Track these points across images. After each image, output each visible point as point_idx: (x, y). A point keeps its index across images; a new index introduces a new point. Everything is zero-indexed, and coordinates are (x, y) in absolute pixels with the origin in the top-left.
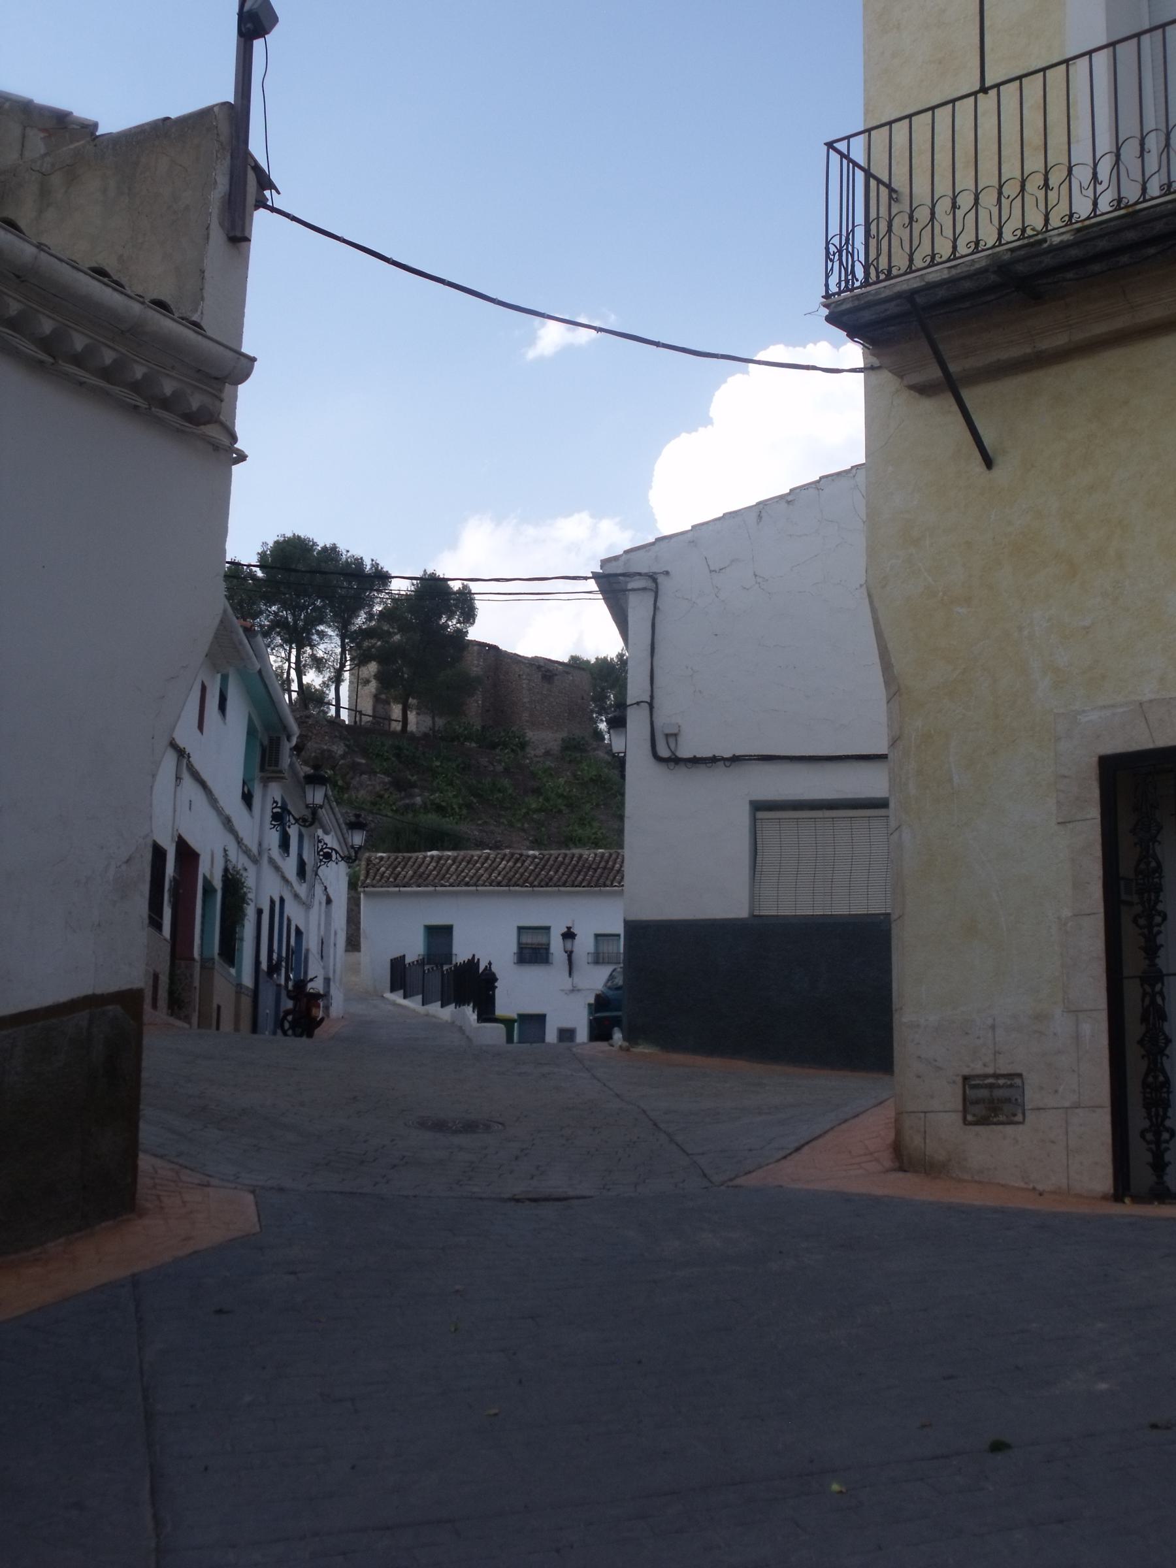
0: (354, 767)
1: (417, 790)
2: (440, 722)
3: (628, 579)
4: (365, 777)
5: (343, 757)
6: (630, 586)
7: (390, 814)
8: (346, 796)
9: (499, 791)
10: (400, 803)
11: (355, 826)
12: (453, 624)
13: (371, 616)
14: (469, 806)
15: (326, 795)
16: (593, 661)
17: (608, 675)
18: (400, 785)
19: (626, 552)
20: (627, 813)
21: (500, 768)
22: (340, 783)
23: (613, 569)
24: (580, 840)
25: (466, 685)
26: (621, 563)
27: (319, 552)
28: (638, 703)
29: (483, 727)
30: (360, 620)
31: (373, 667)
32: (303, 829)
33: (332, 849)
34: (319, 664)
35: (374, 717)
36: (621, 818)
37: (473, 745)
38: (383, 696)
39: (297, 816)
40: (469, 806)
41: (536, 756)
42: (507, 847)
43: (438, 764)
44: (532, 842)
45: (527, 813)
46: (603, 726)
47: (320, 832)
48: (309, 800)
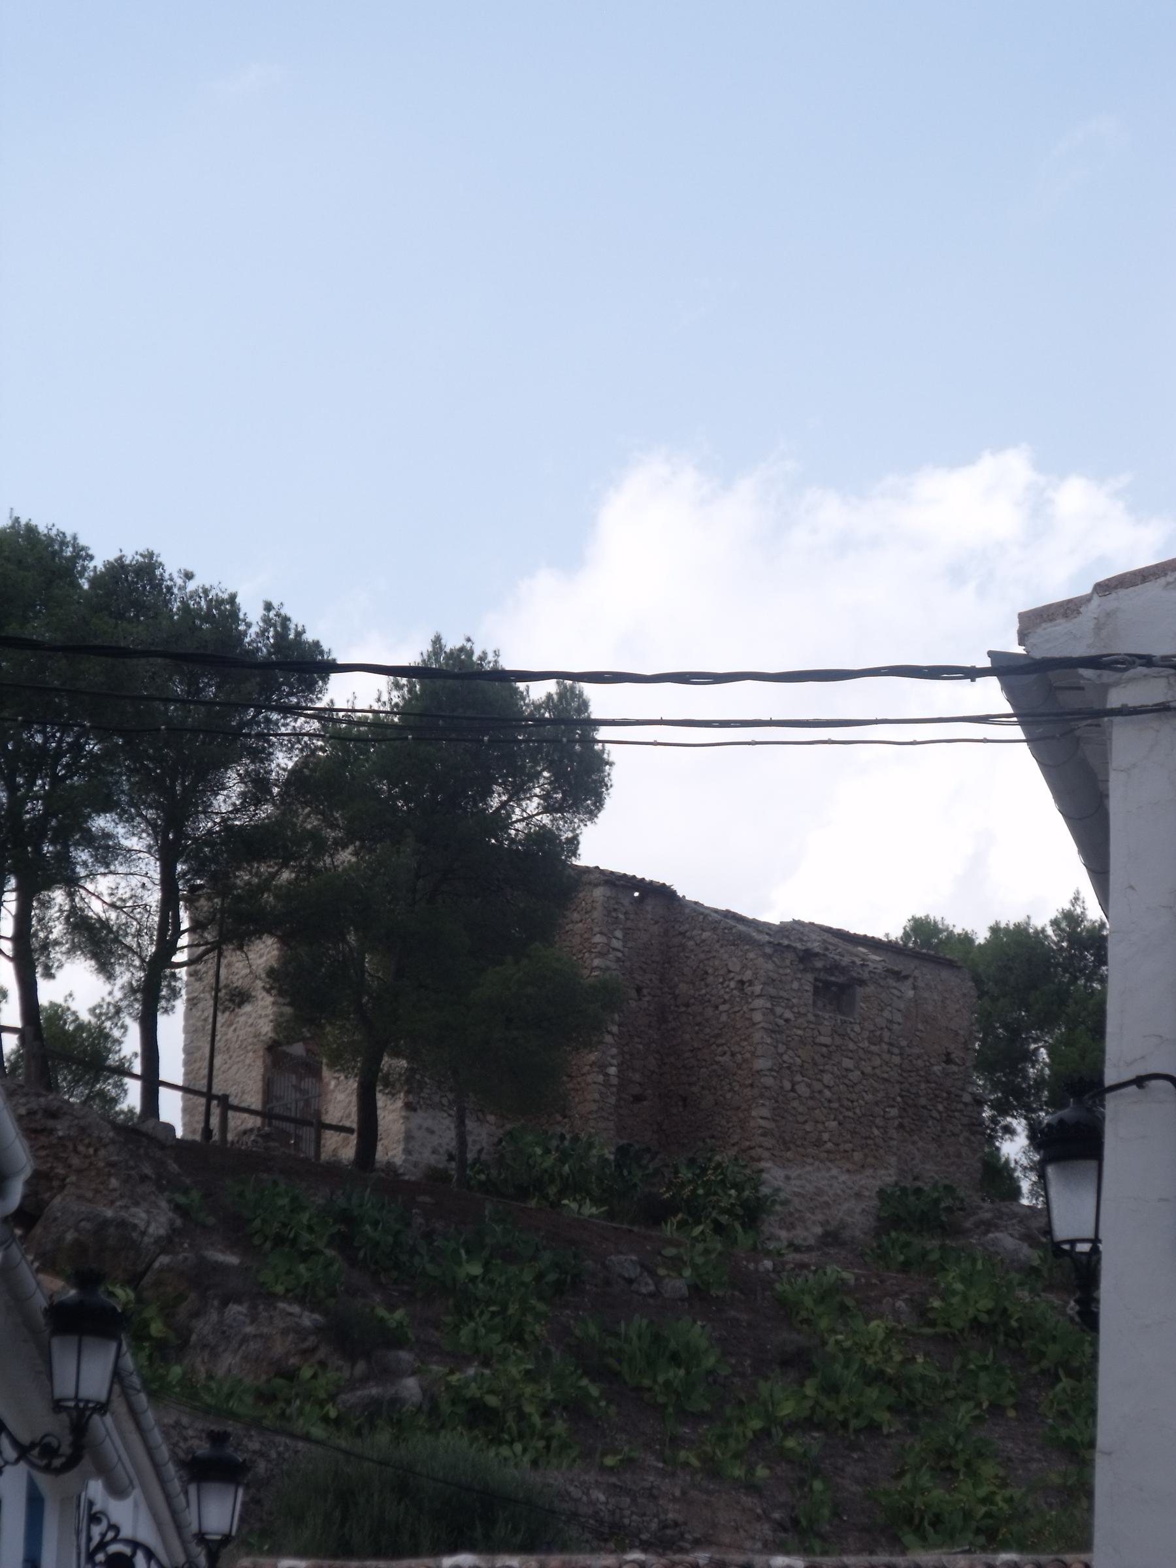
0: (203, 1278)
1: (405, 1356)
2: (483, 1134)
3: (1107, 676)
4: (236, 1310)
5: (167, 1244)
6: (1115, 699)
7: (318, 1432)
8: (176, 1371)
9: (675, 1359)
10: (350, 1398)
11: (209, 1469)
12: (530, 812)
13: (258, 788)
14: (576, 1409)
15: (117, 1375)
16: (982, 936)
17: (1035, 989)
18: (351, 1338)
19: (1104, 588)
20: (1103, 1439)
21: (676, 1285)
22: (157, 1328)
23: (1072, 641)
24: (937, 1521)
25: (567, 1012)
26: (1086, 620)
27: (97, 581)
28: (1140, 1081)
29: (622, 1151)
30: (228, 797)
31: (265, 952)
32: (44, 1481)
33: (135, 1545)
34: (97, 941)
35: (266, 1114)
36: (1079, 1452)
37: (589, 1210)
38: (298, 1049)
39: (25, 1438)
40: (576, 1409)
41: (794, 1247)
42: (698, 1543)
43: (476, 1270)
44: (780, 1526)
45: (766, 1433)
46: (1014, 1148)
47: (96, 1489)
48: (64, 1387)
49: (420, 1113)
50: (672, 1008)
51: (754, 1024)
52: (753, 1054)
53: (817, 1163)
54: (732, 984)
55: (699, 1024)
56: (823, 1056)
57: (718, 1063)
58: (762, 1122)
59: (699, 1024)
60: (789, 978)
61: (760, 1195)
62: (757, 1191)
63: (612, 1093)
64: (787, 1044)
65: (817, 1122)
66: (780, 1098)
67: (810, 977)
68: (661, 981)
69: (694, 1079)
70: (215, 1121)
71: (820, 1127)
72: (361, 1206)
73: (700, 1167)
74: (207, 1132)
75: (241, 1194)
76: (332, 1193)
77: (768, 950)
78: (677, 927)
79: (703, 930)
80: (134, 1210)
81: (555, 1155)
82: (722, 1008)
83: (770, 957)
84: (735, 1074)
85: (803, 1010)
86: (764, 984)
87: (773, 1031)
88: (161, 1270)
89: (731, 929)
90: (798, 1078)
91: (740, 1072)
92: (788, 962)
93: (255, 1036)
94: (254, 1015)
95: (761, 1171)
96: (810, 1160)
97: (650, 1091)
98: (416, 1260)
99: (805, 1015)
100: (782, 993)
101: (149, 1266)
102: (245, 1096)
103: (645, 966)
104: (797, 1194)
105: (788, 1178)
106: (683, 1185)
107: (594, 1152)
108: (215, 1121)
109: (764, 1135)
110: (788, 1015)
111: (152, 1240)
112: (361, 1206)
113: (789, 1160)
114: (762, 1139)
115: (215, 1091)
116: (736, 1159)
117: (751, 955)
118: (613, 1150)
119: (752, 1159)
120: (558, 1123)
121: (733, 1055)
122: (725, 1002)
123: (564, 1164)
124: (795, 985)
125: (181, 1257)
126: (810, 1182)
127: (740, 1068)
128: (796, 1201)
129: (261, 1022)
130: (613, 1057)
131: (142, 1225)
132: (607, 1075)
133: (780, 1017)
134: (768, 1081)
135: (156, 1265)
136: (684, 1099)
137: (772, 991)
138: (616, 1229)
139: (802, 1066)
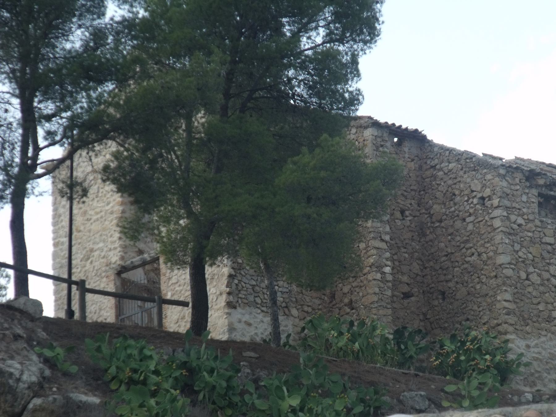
5: (38, 389)
29: (399, 333)
31: (106, 153)
49: (239, 310)
50: (429, 224)
51: (495, 229)
52: (495, 252)
53: (549, 334)
54: (475, 201)
55: (451, 234)
56: (549, 252)
57: (467, 262)
58: (506, 304)
59: (451, 234)
60: (519, 193)
61: (509, 359)
62: (506, 357)
63: (388, 287)
64: (521, 244)
65: (547, 303)
66: (519, 285)
67: (535, 192)
68: (419, 205)
69: (450, 277)
70: (76, 307)
71: (550, 307)
72: (198, 359)
73: (460, 341)
74: (70, 313)
75: (99, 349)
76: (174, 351)
77: (502, 171)
78: (428, 162)
79: (450, 163)
80: (10, 362)
81: (347, 336)
82: (469, 220)
83: (504, 177)
84: (482, 270)
85: (531, 217)
86: (500, 197)
87: (510, 234)
88: (35, 410)
89: (471, 158)
90: (531, 269)
91: (486, 267)
92: (517, 181)
93: (107, 266)
94: (105, 249)
95: (507, 341)
96: (544, 333)
97: (416, 290)
98: (247, 397)
99: (533, 221)
100: (514, 205)
101: (25, 408)
102: (102, 312)
103: (405, 193)
104: (536, 359)
105: (528, 346)
106: (448, 354)
107: (378, 332)
108: (76, 307)
109: (508, 314)
110: (520, 221)
111: (26, 386)
112: (198, 359)
113: (528, 333)
114: (506, 317)
115: (74, 278)
116: (487, 333)
117: (489, 177)
118: (392, 331)
119: (500, 333)
120: (348, 314)
121: (479, 255)
122: (470, 215)
123: (354, 343)
124: (524, 198)
125: (51, 399)
126: (545, 349)
127: (486, 265)
128: (535, 363)
129: (111, 253)
130: (387, 259)
131: (17, 374)
132: (383, 273)
133: (514, 222)
134: (509, 272)
135: (31, 406)
136: (443, 293)
137: (507, 203)
138: (406, 374)
139: (533, 261)
